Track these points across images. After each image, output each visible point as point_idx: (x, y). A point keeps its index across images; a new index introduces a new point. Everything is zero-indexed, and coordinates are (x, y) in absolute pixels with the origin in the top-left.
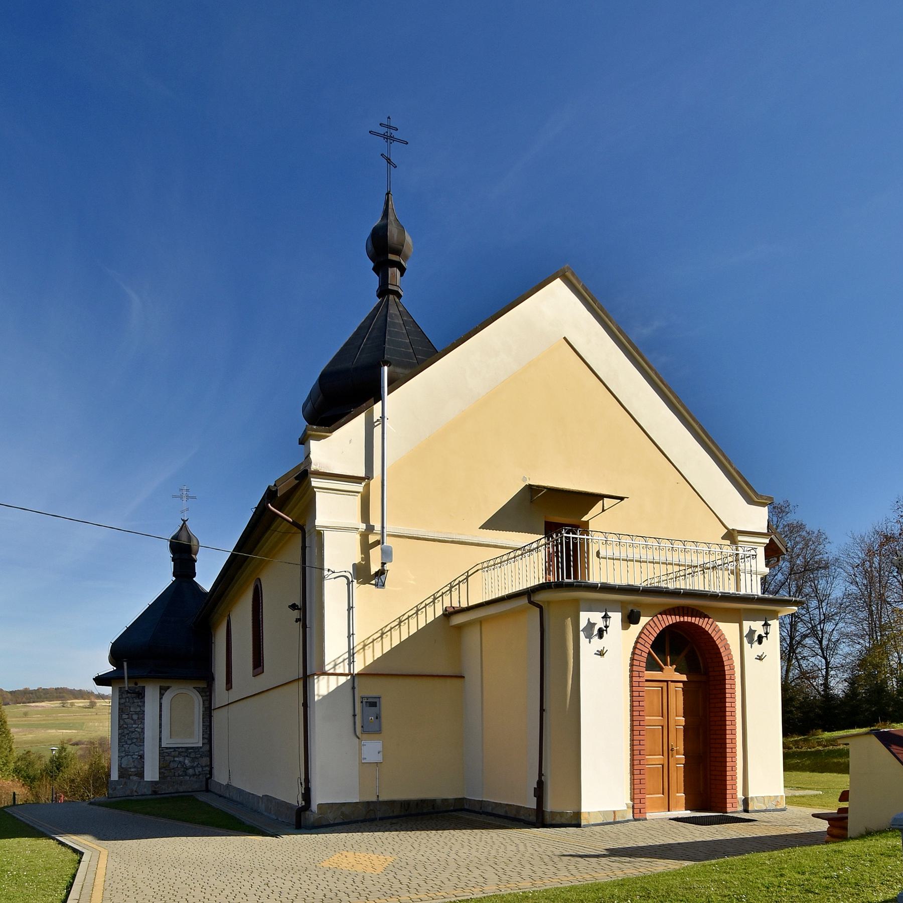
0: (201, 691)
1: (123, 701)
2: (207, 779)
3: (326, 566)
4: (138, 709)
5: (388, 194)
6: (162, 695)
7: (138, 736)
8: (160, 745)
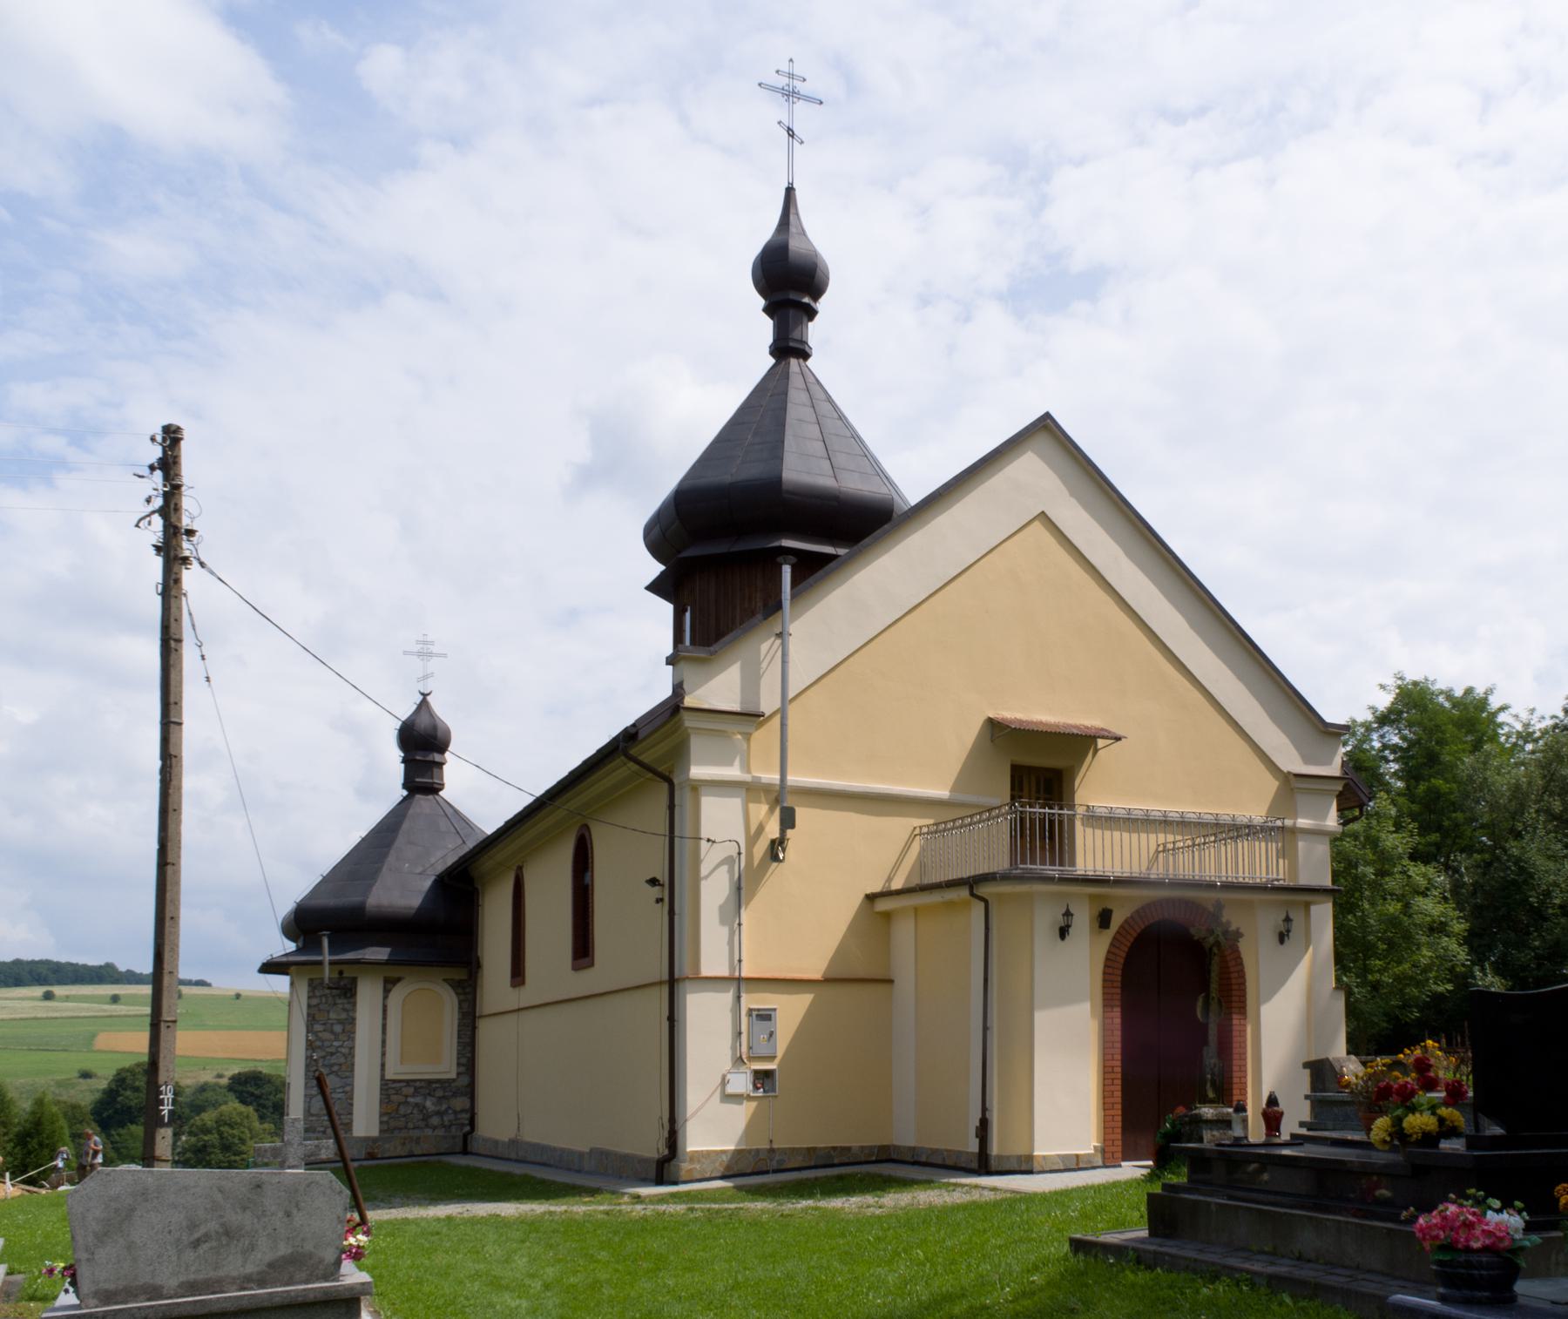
0: (457, 986)
1: (315, 1001)
2: (465, 1137)
3: (704, 834)
4: (344, 1016)
5: (790, 191)
6: (387, 992)
7: (342, 1060)
8: (383, 1076)
